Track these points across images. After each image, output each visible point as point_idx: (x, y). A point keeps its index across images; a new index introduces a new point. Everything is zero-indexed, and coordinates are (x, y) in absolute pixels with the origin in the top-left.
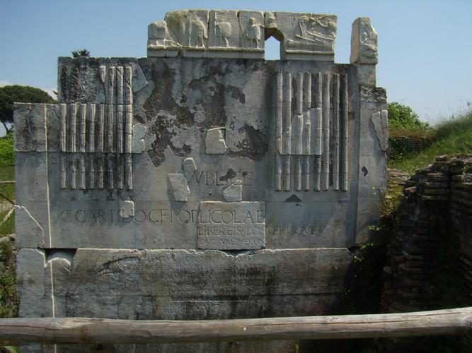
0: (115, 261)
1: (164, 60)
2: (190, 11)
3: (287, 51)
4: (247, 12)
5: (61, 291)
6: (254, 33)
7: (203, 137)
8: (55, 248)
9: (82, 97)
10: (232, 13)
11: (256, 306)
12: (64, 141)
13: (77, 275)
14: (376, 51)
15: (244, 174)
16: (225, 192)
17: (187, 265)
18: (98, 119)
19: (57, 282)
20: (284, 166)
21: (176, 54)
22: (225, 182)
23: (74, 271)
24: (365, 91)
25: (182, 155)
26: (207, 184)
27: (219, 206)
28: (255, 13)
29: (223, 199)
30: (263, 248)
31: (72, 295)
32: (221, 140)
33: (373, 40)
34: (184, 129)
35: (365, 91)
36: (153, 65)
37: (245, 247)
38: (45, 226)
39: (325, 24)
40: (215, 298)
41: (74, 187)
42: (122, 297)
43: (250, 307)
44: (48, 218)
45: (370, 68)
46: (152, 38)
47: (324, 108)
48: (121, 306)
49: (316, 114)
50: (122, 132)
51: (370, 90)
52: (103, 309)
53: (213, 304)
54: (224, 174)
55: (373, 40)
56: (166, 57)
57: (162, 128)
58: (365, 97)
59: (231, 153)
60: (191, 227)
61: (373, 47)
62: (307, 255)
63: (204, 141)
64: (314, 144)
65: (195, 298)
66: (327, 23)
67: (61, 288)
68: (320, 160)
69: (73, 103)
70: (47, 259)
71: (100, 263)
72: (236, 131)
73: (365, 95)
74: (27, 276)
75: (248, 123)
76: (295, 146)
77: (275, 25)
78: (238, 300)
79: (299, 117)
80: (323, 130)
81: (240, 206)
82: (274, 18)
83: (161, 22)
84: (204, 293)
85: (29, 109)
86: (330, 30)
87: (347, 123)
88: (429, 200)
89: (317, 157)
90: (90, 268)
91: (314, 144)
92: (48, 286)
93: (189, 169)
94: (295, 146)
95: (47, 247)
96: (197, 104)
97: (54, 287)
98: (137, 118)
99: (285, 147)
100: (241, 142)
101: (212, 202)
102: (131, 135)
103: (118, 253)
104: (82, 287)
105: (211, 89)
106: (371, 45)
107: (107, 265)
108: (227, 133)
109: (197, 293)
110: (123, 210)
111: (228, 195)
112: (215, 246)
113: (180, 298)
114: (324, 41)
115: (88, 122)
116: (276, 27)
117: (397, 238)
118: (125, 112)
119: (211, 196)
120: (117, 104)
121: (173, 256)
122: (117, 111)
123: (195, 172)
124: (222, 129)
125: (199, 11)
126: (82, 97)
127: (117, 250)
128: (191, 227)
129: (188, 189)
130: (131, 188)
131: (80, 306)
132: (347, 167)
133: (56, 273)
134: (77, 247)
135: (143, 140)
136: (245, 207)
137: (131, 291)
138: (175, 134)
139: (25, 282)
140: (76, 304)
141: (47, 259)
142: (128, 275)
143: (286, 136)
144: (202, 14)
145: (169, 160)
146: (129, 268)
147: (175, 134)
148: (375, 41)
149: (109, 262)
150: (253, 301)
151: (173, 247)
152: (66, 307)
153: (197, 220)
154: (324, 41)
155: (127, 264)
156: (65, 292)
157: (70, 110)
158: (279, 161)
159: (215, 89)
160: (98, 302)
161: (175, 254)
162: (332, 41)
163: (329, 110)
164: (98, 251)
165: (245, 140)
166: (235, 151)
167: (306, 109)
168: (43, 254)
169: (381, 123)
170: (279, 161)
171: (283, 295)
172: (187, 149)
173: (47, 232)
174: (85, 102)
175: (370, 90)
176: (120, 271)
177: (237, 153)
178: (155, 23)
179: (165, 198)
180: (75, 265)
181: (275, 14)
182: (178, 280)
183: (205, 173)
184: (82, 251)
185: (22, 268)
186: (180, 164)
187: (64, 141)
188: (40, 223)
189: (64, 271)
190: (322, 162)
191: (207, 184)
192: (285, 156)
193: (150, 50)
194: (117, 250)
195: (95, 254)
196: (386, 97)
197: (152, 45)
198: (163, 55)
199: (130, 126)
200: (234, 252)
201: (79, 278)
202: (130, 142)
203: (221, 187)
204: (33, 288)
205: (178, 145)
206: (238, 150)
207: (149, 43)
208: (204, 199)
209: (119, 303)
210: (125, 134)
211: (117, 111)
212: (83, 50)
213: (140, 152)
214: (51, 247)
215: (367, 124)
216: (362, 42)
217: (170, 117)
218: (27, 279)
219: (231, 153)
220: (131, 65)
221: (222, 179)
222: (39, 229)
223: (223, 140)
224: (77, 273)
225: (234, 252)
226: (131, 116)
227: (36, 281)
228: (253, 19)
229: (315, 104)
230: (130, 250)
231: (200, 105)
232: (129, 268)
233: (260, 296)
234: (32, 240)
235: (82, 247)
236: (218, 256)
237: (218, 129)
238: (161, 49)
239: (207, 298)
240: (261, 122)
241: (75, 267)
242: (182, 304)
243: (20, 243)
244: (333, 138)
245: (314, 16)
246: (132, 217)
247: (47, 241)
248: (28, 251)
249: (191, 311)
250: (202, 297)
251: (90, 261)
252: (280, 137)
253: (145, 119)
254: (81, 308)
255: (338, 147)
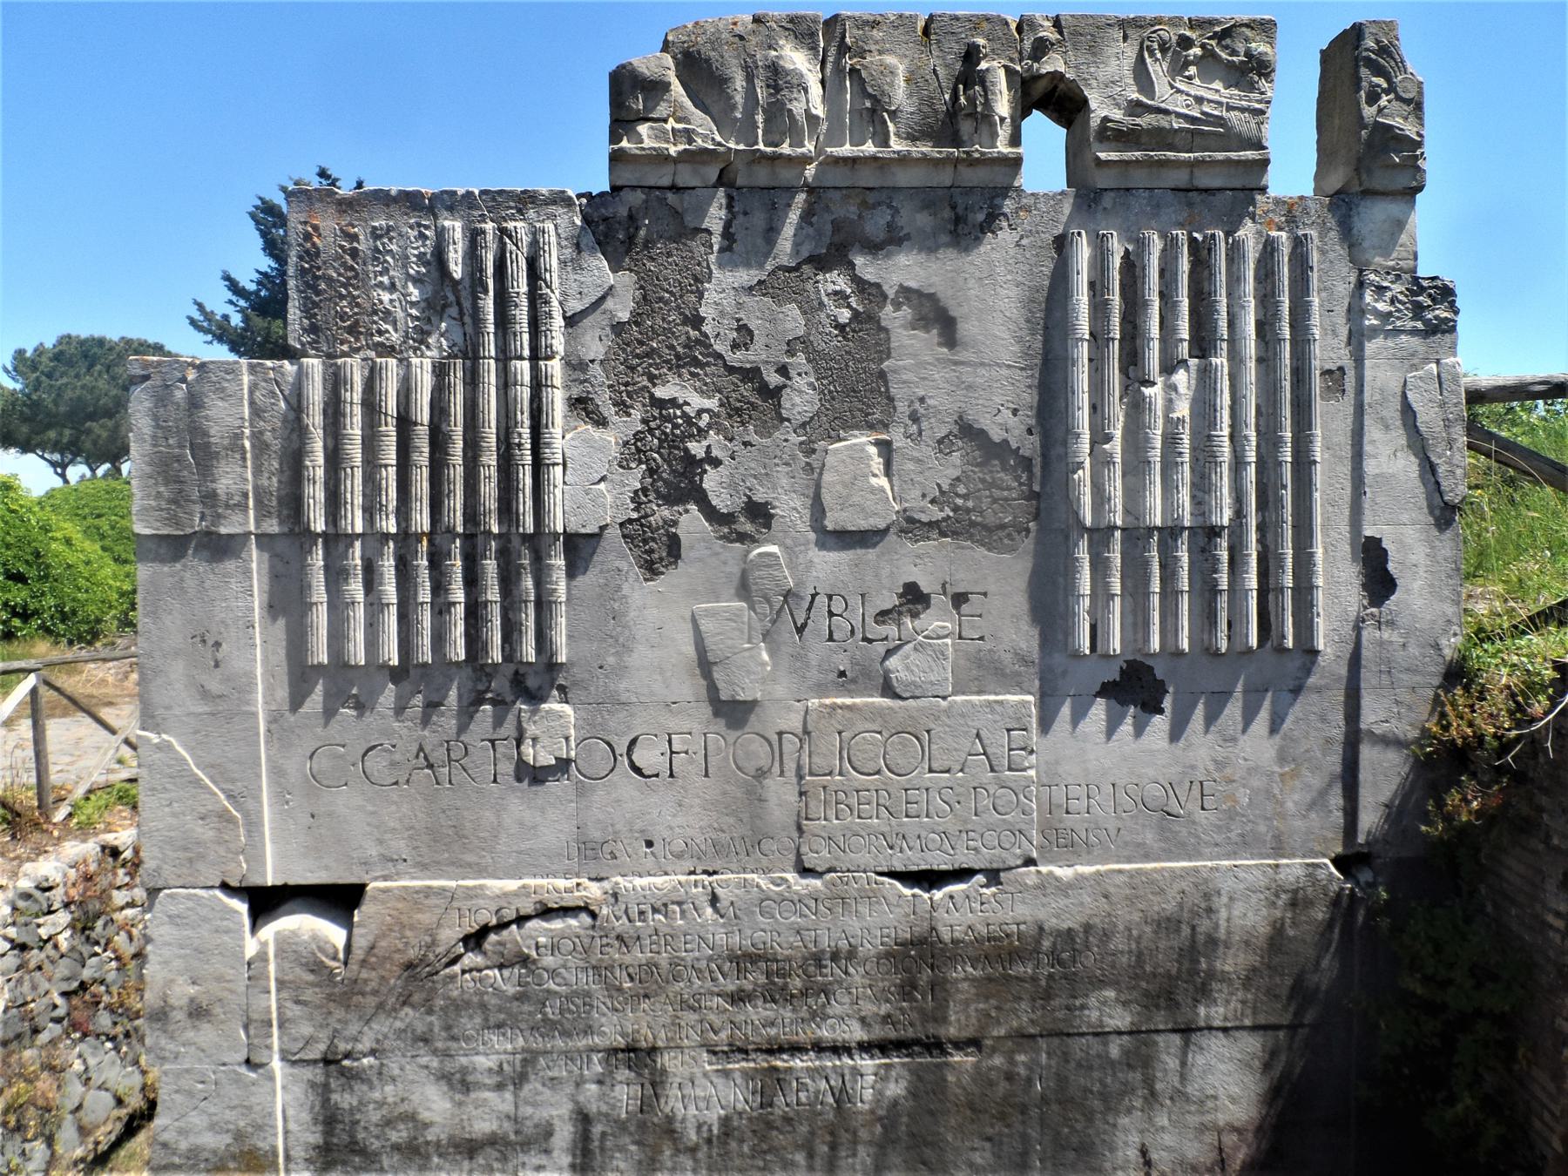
0: (506, 925)
1: (671, 197)
2: (757, 20)
3: (1103, 155)
4: (956, 18)
5: (309, 1041)
6: (1071, 99)
7: (814, 472)
8: (285, 886)
9: (380, 333)
10: (904, 22)
11: (1010, 1077)
12: (315, 495)
13: (366, 981)
14: (1419, 144)
15: (959, 599)
16: (893, 662)
17: (760, 933)
18: (439, 408)
19: (294, 1011)
20: (1100, 567)
21: (712, 174)
22: (890, 630)
23: (354, 967)
24: (1380, 290)
25: (742, 537)
26: (831, 639)
27: (877, 713)
28: (988, 19)
29: (888, 690)
30: (1030, 862)
31: (347, 1056)
32: (873, 481)
33: (1408, 102)
34: (746, 444)
35: (1380, 290)
36: (631, 217)
37: (964, 860)
38: (1543, 732)
39: (1234, 53)
40: (866, 1047)
41: (1223, 645)
42: (530, 1059)
43: (991, 1084)
44: (259, 776)
45: (1392, 208)
46: (622, 123)
47: (1235, 358)
48: (527, 1089)
49: (1206, 378)
50: (528, 459)
51: (1397, 288)
52: (460, 1104)
53: (857, 1072)
54: (890, 600)
55: (1408, 102)
56: (674, 188)
57: (671, 443)
58: (1378, 314)
59: (911, 526)
60: (781, 794)
61: (1410, 130)
62: (1184, 885)
63: (818, 487)
64: (1202, 487)
65: (795, 1049)
66: (1242, 51)
67: (306, 1029)
68: (1224, 543)
69: (344, 354)
70: (254, 927)
71: (450, 935)
72: (927, 451)
73: (1382, 306)
74: (183, 992)
75: (970, 417)
76: (1134, 496)
77: (1053, 63)
78: (944, 1053)
79: (1147, 391)
80: (1232, 437)
81: (947, 712)
82: (1052, 35)
83: (655, 63)
84: (825, 1033)
85: (184, 380)
86: (1250, 72)
87: (1319, 406)
88: (1245, 685)
89: (1214, 532)
90: (412, 954)
91: (1202, 487)
92: (256, 1025)
93: (768, 584)
94: (1134, 496)
95: (255, 880)
96: (791, 353)
97: (280, 1027)
98: (581, 405)
99: (1101, 498)
100: (945, 487)
101: (848, 701)
102: (559, 469)
103: (516, 894)
104: (381, 1026)
105: (839, 295)
106: (1397, 122)
107: (475, 940)
108: (896, 458)
109: (803, 1036)
110: (535, 740)
111: (903, 675)
112: (864, 858)
113: (740, 1050)
114: (1233, 116)
115: (405, 423)
116: (1062, 69)
117: (118, 916)
118: (538, 385)
119: (844, 680)
120: (505, 357)
121: (714, 900)
122: (506, 383)
123: (788, 594)
124: (878, 443)
125: (792, 20)
126: (380, 333)
127: (512, 885)
128: (781, 794)
129: (765, 656)
130: (562, 658)
131: (377, 1095)
132: (1319, 568)
133: (290, 977)
134: (364, 879)
135: (602, 486)
136: (963, 715)
137: (566, 1034)
138: (716, 463)
139: (178, 1015)
140: (360, 1088)
141: (254, 927)
142: (553, 973)
143: (1101, 462)
144: (800, 30)
145: (693, 554)
146: (554, 948)
147: (716, 463)
148: (1416, 106)
149: (484, 931)
150: (998, 1061)
151: (717, 865)
152: (326, 1101)
153: (799, 768)
154: (1233, 116)
155: (550, 934)
156: (322, 1047)
157: (336, 383)
158: (1083, 554)
159: (853, 301)
160: (445, 1077)
161: (719, 891)
162: (1262, 112)
163: (1251, 365)
164: (444, 889)
165: (958, 479)
166: (925, 518)
167: (1168, 368)
168: (242, 907)
169: (1442, 405)
170: (1083, 554)
171: (1101, 1034)
172: (760, 513)
173: (254, 825)
174: (388, 350)
175: (1397, 288)
176: (524, 960)
177: (931, 525)
178: (636, 61)
179: (688, 688)
180: (360, 943)
181: (1057, 23)
182: (731, 987)
183: (822, 600)
184: (385, 891)
185: (166, 962)
186: (735, 570)
187: (315, 495)
188: (230, 797)
189: (316, 967)
190: (1232, 550)
191: (831, 639)
192: (1100, 535)
193: (616, 158)
194: (512, 885)
195: (433, 901)
196: (1456, 312)
197: (624, 144)
198: (666, 182)
199: (563, 435)
200: (929, 879)
201: (375, 993)
202: (558, 492)
203: (880, 648)
204: (206, 1034)
205: (722, 501)
206: (936, 514)
207: (614, 138)
208: (821, 689)
209: (520, 1080)
210: (539, 466)
211: (506, 383)
212: (317, 170)
213: (592, 528)
214: (270, 880)
215: (1393, 411)
216: (1369, 112)
217: (696, 401)
218: (184, 1001)
219: (911, 526)
220: (553, 217)
221: (883, 616)
222: (224, 816)
223: (883, 482)
224: (364, 974)
225: (929, 879)
226: (557, 400)
227: (217, 1010)
228: (981, 41)
229: (1203, 344)
230: (561, 883)
231: (801, 358)
232: (554, 948)
233: (1022, 1038)
234: (201, 857)
235: (385, 878)
236: (870, 896)
237: (862, 440)
238: (661, 158)
239: (838, 1049)
240: (1015, 412)
241: (358, 954)
242: (747, 1075)
243: (158, 870)
244: (1267, 464)
245: (1194, 24)
246: (568, 761)
247: (257, 859)
248: (189, 897)
249: (780, 1100)
250: (819, 1048)
251: (412, 927)
252: (1080, 465)
253: (609, 411)
254: (381, 1104)
255: (1287, 495)
